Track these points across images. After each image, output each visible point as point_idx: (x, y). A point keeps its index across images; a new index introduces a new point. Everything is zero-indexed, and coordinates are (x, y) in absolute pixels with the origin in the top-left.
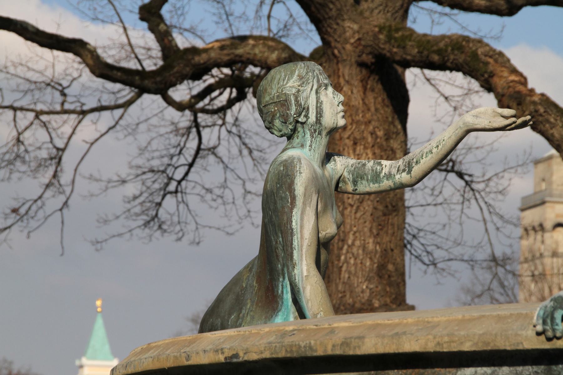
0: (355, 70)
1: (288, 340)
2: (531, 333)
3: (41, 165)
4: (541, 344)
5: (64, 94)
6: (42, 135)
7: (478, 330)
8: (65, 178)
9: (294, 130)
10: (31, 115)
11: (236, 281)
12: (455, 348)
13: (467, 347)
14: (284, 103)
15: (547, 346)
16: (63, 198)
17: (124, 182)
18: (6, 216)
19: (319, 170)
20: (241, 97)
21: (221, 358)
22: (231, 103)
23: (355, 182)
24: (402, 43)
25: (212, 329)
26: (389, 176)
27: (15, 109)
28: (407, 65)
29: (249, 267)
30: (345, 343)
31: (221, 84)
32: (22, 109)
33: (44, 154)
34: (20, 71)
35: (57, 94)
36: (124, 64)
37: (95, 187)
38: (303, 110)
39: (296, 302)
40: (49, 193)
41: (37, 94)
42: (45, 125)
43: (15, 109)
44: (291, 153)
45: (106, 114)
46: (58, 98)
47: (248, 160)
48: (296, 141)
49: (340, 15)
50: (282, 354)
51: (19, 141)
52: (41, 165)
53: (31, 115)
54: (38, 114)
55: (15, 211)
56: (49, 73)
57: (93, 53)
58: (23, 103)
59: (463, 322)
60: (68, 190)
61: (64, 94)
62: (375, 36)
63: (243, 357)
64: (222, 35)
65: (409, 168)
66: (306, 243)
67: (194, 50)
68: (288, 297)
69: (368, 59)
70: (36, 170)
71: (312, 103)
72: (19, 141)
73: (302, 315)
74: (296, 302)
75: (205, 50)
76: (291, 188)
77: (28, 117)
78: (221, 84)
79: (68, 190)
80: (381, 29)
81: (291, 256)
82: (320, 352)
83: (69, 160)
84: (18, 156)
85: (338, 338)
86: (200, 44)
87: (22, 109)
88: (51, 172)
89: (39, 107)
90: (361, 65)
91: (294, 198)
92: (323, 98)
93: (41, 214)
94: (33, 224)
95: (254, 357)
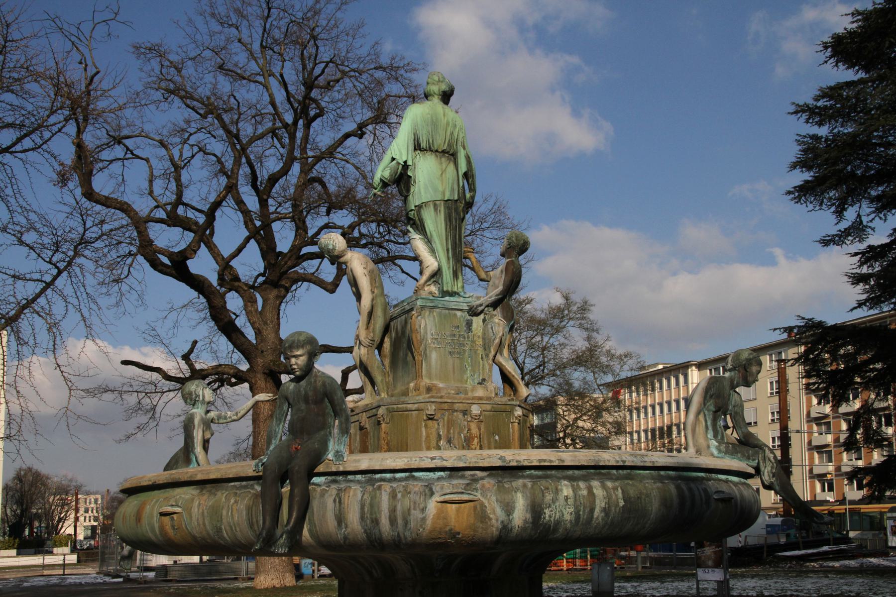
0: (262, 375)
1: (173, 476)
2: (251, 471)
3: (147, 411)
4: (255, 474)
5: (156, 386)
6: (148, 401)
7: (234, 470)
8: (157, 415)
9: (195, 403)
10: (144, 394)
11: (176, 454)
12: (227, 476)
13: (231, 476)
14: (190, 394)
15: (257, 474)
16: (156, 423)
17: (180, 416)
18: (135, 430)
19: (204, 416)
20: (222, 385)
21: (151, 483)
22: (219, 387)
23: (218, 420)
24: (278, 366)
25: (167, 470)
26: (230, 417)
27: (138, 392)
28: (281, 373)
29: (181, 450)
30: (191, 477)
31: (215, 381)
32: (140, 392)
33: (149, 407)
34: (140, 379)
35: (153, 387)
36: (178, 376)
37: (169, 418)
38: (198, 396)
39: (197, 461)
40: (151, 421)
41: (146, 386)
42: (149, 397)
43: (138, 392)
44: (193, 411)
45: (171, 393)
46: (154, 387)
47: (226, 407)
48: (196, 407)
49: (256, 357)
50: (170, 481)
51: (139, 403)
52: (147, 411)
53: (144, 394)
54: (146, 393)
55: (138, 427)
56: (150, 379)
57: (164, 372)
58: (141, 389)
59: (231, 468)
60: (158, 420)
61: (156, 386)
62: (269, 364)
63: (158, 482)
64: (214, 364)
65: (237, 414)
66: (199, 441)
67: (202, 370)
68: (194, 459)
69: (267, 371)
70: (146, 413)
71: (201, 393)
72: (139, 403)
73: (199, 465)
74: (197, 461)
75: (206, 370)
76: (193, 422)
77: (141, 395)
78: (215, 381)
79: (158, 420)
80: (271, 361)
81: (194, 445)
82: (183, 480)
83: (158, 409)
84: (139, 409)
85: (189, 475)
86: (206, 367)
87: (140, 392)
88: (152, 413)
89: (147, 391)
90: (264, 373)
91: (194, 426)
92: (205, 392)
93: (148, 428)
94: (145, 432)
95: (161, 482)
